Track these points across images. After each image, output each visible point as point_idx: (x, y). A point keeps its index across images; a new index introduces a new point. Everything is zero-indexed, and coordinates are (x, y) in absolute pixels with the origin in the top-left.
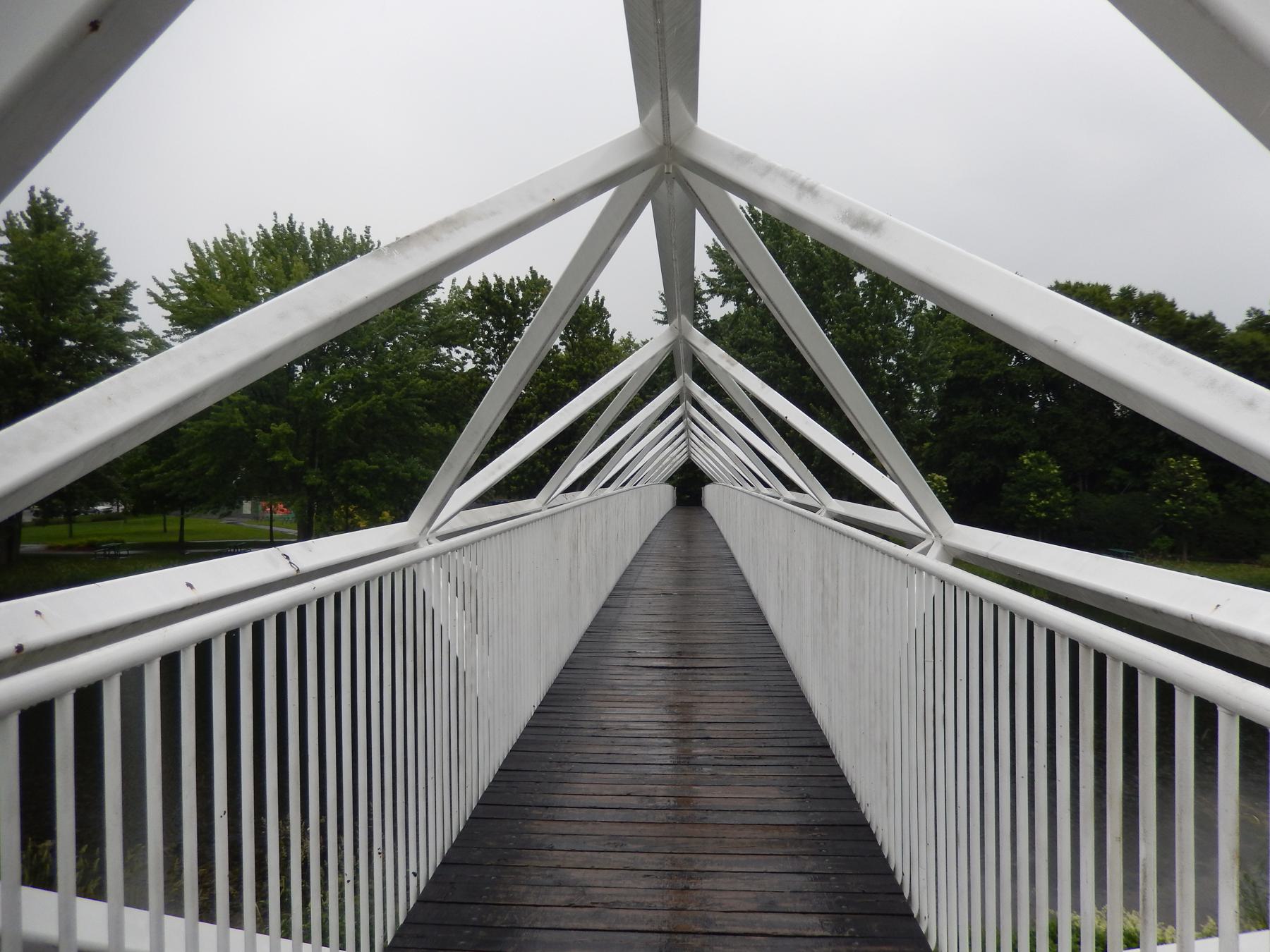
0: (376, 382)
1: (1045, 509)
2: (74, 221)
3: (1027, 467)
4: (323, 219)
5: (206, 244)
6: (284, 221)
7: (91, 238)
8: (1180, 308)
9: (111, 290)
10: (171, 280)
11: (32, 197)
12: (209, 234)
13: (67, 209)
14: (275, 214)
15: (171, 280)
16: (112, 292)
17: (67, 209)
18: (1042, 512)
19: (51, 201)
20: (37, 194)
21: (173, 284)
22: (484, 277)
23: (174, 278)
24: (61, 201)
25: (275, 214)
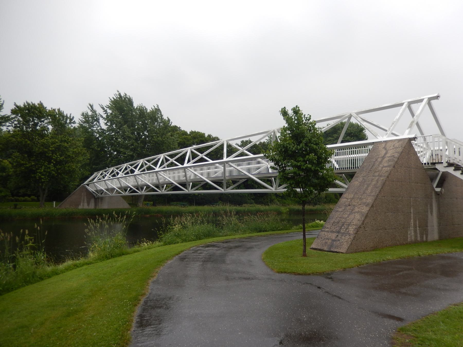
14: (109, 98)
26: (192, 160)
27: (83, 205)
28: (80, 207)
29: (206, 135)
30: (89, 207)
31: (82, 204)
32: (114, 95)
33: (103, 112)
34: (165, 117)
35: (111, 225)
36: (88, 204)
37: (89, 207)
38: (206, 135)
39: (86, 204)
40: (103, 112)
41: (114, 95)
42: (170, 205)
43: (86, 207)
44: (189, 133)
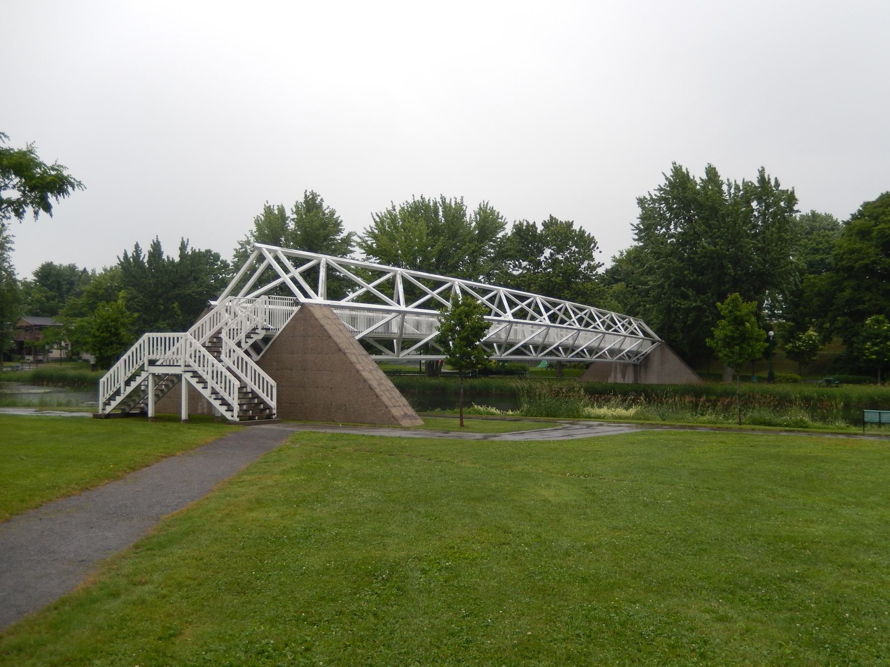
0: (9, 354)
1: (876, 353)
2: (325, 206)
3: (868, 326)
4: (462, 197)
5: (381, 214)
6: (417, 198)
7: (333, 213)
8: (55, 263)
9: (342, 238)
10: (364, 233)
11: (306, 196)
12: (382, 208)
13: (322, 200)
14: (413, 195)
15: (364, 233)
16: (342, 239)
17: (322, 200)
18: (873, 355)
19: (314, 196)
20: (308, 194)
21: (365, 235)
22: (573, 222)
23: (633, 228)
24: (319, 196)
25: (413, 195)
26: (248, 350)
27: (615, 377)
28: (611, 380)
29: (471, 213)
30: (624, 380)
31: (612, 375)
32: (86, 188)
33: (590, 234)
34: (656, 194)
35: (589, 410)
36: (624, 377)
37: (624, 380)
38: (471, 213)
39: (619, 375)
40: (590, 234)
41: (86, 188)
42: (774, 383)
43: (620, 380)
44: (540, 228)
